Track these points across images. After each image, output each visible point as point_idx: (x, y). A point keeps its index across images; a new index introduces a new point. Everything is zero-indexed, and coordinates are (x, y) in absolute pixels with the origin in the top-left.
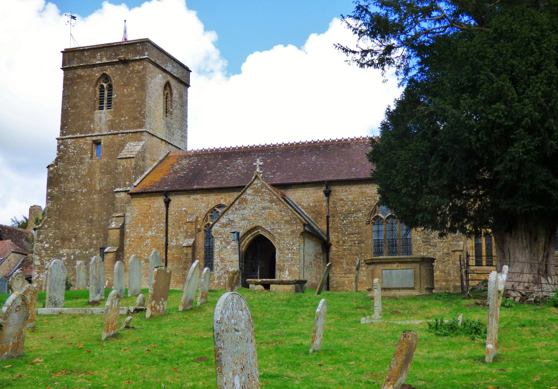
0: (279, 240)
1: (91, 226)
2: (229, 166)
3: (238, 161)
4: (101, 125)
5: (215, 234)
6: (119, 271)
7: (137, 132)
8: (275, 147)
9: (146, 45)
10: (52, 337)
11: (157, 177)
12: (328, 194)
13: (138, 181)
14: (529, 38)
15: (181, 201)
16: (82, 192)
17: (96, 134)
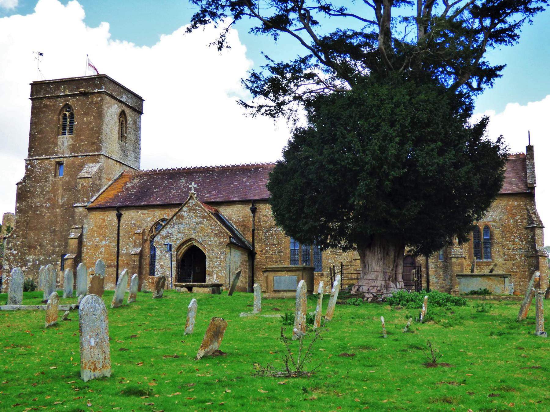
0: (209, 250)
1: (54, 235)
2: (173, 185)
3: (181, 181)
4: (63, 148)
5: (156, 245)
6: (68, 276)
7: (95, 155)
8: (214, 169)
9: (104, 80)
10: (9, 326)
11: (111, 194)
12: (254, 210)
13: (94, 198)
14: (371, 106)
15: (131, 215)
16: (46, 206)
17: (60, 156)
